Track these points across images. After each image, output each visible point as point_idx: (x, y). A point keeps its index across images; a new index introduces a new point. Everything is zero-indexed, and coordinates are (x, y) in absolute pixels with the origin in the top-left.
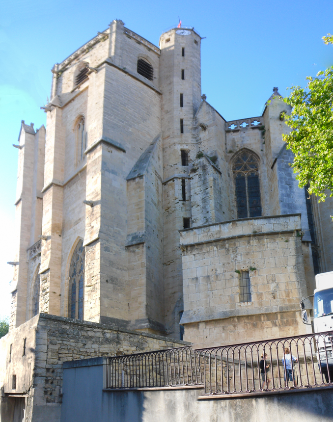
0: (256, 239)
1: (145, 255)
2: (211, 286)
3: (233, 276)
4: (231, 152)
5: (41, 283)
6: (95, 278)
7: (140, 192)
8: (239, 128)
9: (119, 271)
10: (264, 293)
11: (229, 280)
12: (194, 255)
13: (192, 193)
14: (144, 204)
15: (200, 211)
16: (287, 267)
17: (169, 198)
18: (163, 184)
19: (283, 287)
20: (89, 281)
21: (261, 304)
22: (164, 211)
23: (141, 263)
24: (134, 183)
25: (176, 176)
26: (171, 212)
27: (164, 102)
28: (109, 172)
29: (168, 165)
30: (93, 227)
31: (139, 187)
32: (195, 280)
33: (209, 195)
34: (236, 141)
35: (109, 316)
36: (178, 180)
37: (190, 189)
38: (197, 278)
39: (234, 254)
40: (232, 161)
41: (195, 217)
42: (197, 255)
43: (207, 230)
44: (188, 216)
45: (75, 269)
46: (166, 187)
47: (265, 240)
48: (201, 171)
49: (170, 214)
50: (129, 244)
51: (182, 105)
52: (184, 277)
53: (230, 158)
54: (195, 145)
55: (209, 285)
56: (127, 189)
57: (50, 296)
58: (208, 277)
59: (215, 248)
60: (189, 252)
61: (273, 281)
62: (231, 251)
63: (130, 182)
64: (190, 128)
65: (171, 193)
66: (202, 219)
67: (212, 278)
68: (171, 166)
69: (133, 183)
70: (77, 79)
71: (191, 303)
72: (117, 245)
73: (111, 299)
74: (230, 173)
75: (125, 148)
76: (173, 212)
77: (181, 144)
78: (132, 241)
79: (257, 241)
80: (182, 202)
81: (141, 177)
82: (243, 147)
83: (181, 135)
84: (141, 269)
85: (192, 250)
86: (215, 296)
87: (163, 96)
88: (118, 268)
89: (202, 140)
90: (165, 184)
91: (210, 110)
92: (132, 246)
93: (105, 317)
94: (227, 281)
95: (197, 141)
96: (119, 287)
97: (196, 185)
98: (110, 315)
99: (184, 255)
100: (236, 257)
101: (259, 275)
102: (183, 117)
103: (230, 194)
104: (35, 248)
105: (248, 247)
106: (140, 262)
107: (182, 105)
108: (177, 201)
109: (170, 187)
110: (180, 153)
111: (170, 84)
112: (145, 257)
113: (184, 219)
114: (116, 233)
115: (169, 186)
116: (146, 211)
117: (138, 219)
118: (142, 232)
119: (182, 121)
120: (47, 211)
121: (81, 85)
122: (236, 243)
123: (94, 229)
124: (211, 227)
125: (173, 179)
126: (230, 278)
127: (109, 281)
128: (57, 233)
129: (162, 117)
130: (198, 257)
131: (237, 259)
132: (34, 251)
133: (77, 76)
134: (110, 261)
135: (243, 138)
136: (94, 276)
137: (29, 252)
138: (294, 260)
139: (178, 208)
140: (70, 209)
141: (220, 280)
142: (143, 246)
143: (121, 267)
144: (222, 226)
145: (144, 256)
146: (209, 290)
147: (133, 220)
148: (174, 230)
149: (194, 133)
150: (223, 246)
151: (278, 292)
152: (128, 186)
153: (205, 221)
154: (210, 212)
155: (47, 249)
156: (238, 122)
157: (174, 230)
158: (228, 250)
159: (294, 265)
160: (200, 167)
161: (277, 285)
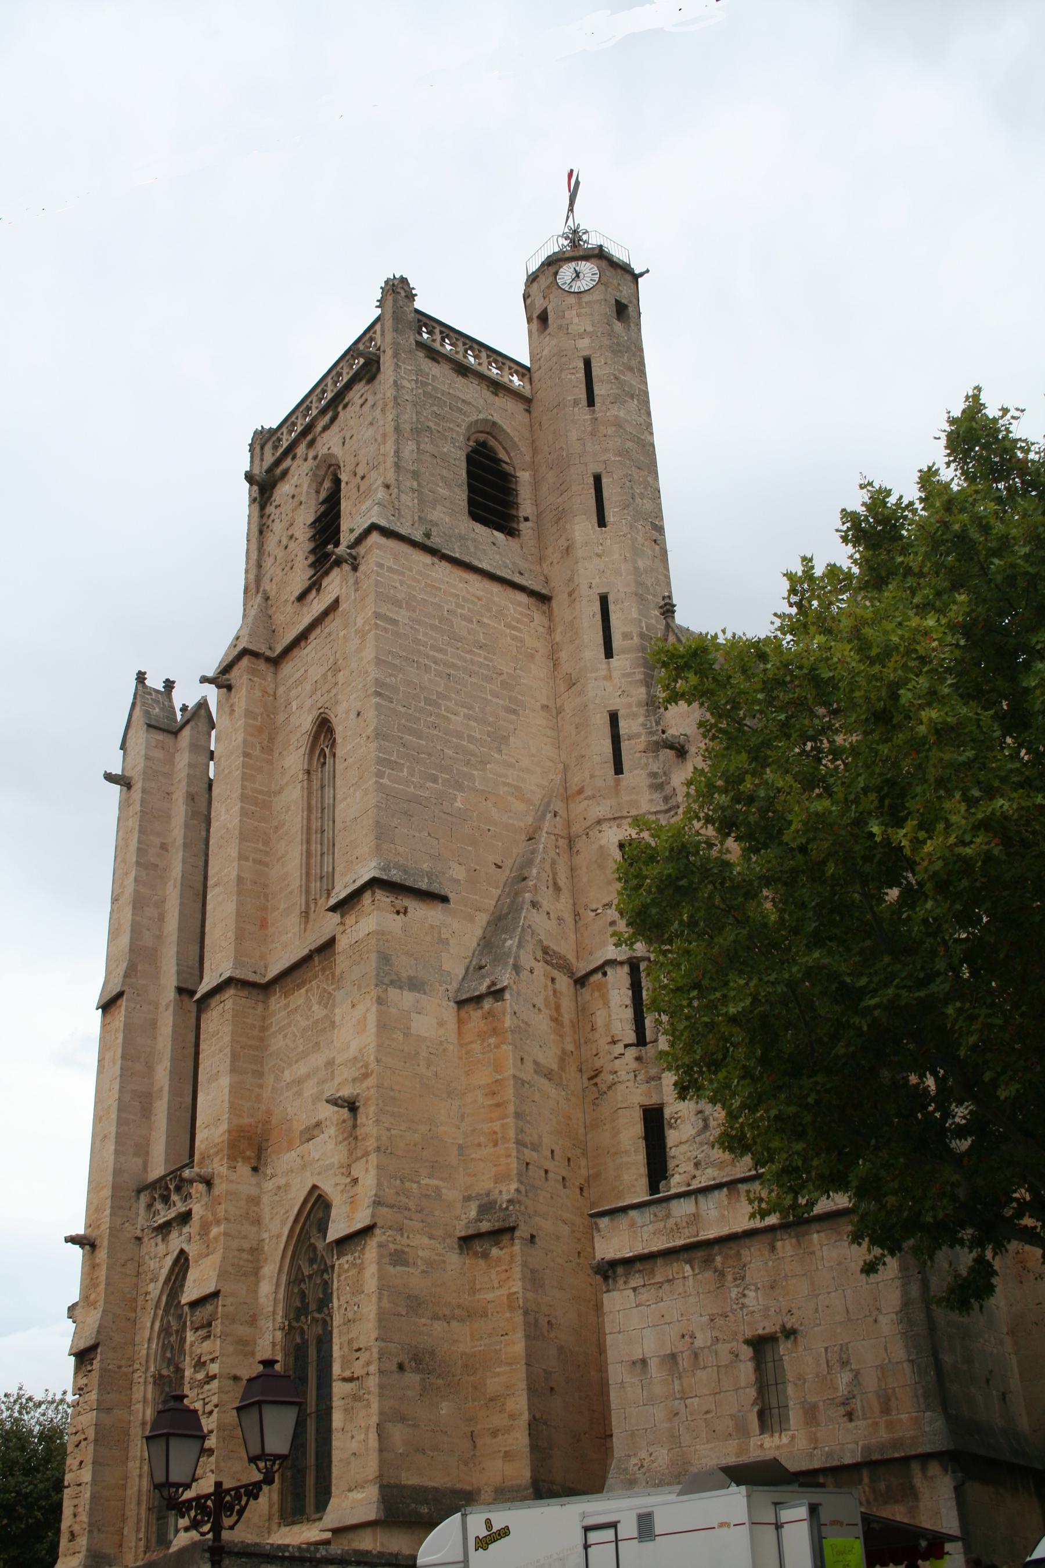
0: (790, 1237)
1: (519, 1269)
2: (682, 1385)
3: (737, 1356)
5: (190, 1337)
6: (364, 1356)
7: (497, 1047)
9: (438, 1326)
10: (821, 1404)
11: (726, 1366)
12: (634, 1289)
14: (509, 1092)
16: (880, 1318)
17: (597, 1035)
18: (576, 982)
19: (870, 1381)
20: (346, 1363)
21: (814, 1440)
22: (586, 1083)
23: (510, 1295)
24: (479, 1013)
28: (401, 988)
30: (355, 1181)
31: (495, 1031)
32: (639, 1365)
35: (410, 1482)
36: (619, 969)
38: (644, 1362)
39: (737, 1286)
42: (642, 1290)
43: (663, 1213)
44: (654, 1100)
45: (303, 1294)
46: (586, 993)
47: (815, 1236)
50: (471, 1232)
52: (611, 1355)
55: (677, 1382)
56: (460, 1033)
57: (221, 1390)
58: (673, 1356)
59: (687, 1267)
60: (621, 1281)
61: (844, 1363)
62: (730, 1277)
64: (642, 747)
66: (693, 1119)
67: (684, 1362)
69: (475, 1016)
71: (633, 1434)
72: (431, 1237)
73: (414, 1426)
79: (794, 1241)
80: (632, 1052)
81: (497, 994)
84: (508, 1315)
85: (627, 1275)
86: (691, 1414)
88: (435, 1317)
92: (479, 1236)
93: (396, 1486)
94: (723, 1370)
95: (666, 799)
96: (440, 1381)
98: (411, 1480)
99: (608, 1291)
100: (744, 1296)
101: (805, 1349)
104: (167, 1188)
105: (770, 1263)
106: (504, 1291)
108: (619, 1048)
112: (519, 1276)
114: (427, 1196)
116: (518, 1115)
117: (496, 1145)
118: (508, 1191)
119: (614, 718)
120: (214, 1078)
122: (742, 1252)
123: (359, 1189)
124: (674, 1204)
126: (731, 1362)
127: (406, 1364)
128: (246, 1159)
130: (645, 1295)
131: (746, 1301)
132: (166, 1199)
133: (314, 522)
134: (409, 1296)
136: (359, 1349)
137: (144, 1199)
138: (898, 1293)
139: (623, 1075)
140: (287, 1076)
141: (705, 1368)
142: (512, 1239)
143: (447, 1312)
144: (701, 1198)
145: (517, 1270)
146: (678, 1396)
147: (479, 1145)
148: (616, 1153)
150: (708, 1261)
151: (858, 1397)
152: (460, 1022)
153: (701, 1124)
155: (211, 1217)
157: (616, 1153)
158: (722, 1274)
159: (898, 1309)
161: (856, 1376)
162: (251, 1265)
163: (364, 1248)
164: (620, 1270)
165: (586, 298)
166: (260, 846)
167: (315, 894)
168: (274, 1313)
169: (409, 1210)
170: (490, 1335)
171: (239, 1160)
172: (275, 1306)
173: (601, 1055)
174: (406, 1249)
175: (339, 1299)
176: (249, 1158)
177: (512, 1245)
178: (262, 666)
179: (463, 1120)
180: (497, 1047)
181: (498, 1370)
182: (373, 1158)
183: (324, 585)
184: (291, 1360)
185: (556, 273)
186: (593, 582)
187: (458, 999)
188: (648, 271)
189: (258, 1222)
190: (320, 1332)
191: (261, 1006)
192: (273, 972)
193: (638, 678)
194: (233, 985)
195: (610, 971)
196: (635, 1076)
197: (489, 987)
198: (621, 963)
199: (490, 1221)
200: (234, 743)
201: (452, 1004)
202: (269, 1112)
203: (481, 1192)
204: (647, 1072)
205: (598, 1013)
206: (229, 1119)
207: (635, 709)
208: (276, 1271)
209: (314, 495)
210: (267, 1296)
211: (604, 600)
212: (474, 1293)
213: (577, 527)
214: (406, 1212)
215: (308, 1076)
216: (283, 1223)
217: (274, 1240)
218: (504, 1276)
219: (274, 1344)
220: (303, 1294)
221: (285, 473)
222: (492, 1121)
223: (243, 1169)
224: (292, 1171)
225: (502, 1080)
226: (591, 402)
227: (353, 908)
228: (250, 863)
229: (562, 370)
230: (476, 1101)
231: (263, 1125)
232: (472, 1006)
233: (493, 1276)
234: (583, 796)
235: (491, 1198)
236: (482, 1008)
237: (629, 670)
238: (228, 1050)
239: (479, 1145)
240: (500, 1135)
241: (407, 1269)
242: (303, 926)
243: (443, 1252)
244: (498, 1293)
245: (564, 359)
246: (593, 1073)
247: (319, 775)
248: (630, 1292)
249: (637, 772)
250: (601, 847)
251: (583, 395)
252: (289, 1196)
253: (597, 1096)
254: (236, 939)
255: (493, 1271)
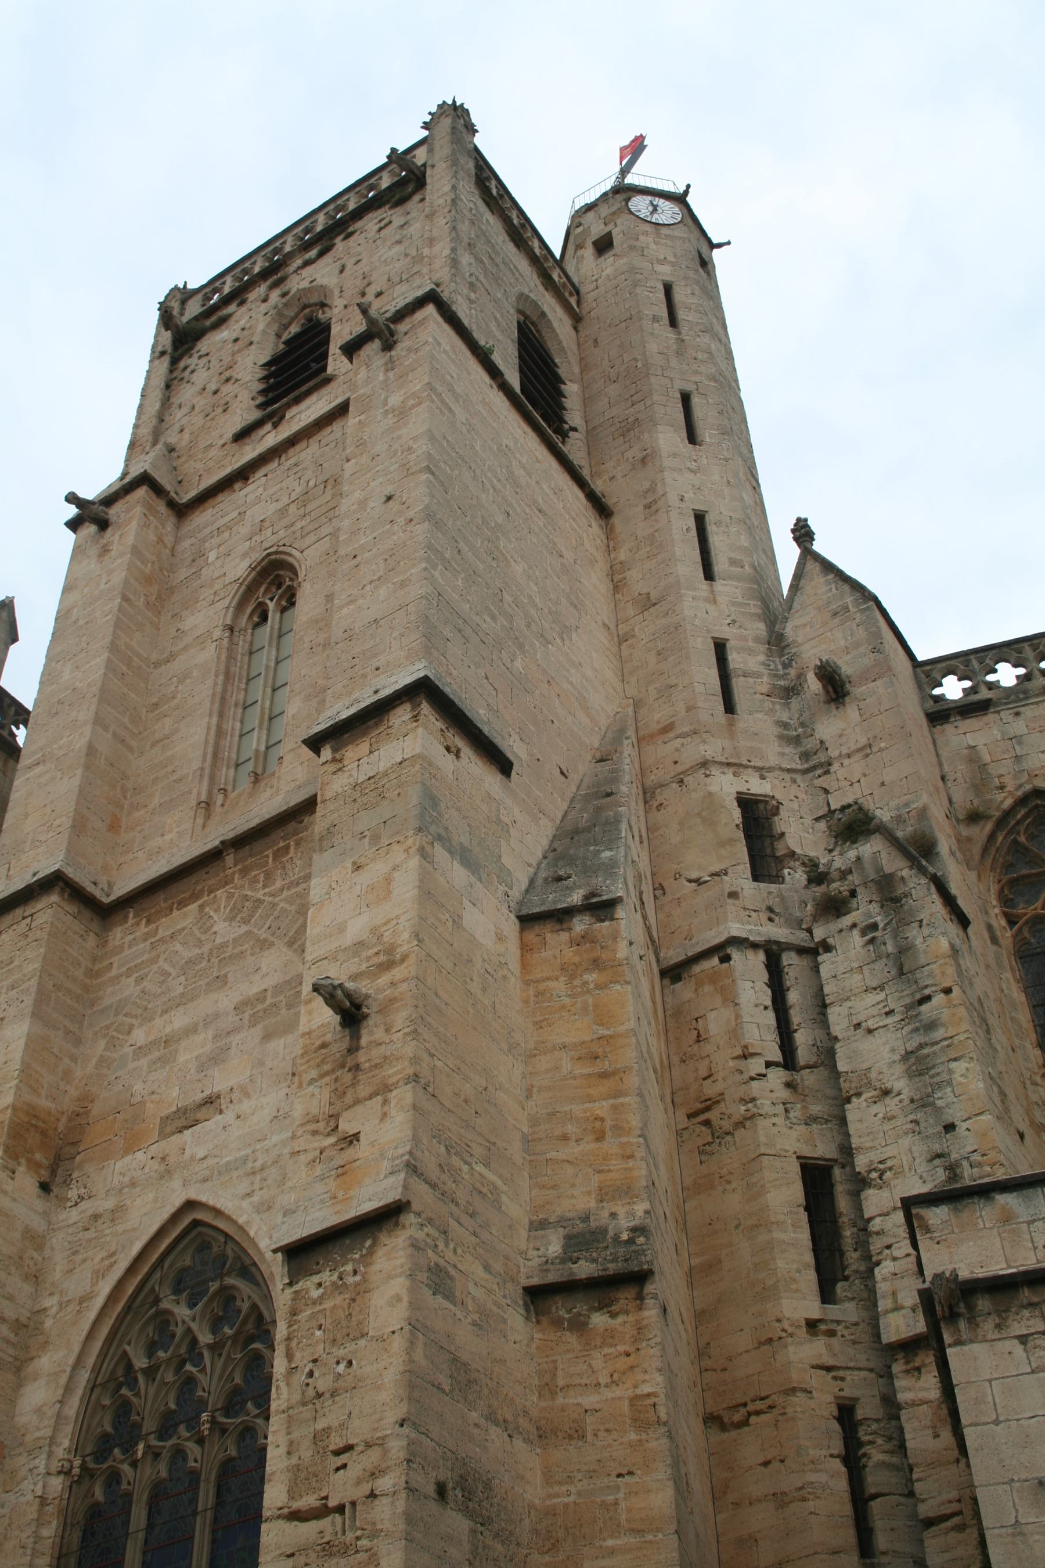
4: (974, 817)
8: (984, 694)
12: (1023, 1339)
13: (838, 1019)
15: (902, 1122)
17: (707, 1048)
18: (664, 973)
23: (634, 1400)
24: (564, 936)
25: (735, 933)
26: (727, 1125)
27: (623, 555)
29: (677, 876)
31: (596, 964)
33: (939, 1034)
34: (987, 758)
36: (750, 954)
37: (825, 1006)
40: (988, 861)
41: (874, 1156)
44: (824, 1149)
45: (123, 1408)
46: (684, 990)
48: (875, 908)
49: (719, 1136)
50: (552, 1278)
51: (709, 574)
53: (977, 849)
54: (799, 778)
56: (524, 965)
60: (988, 1326)
63: (537, 929)
64: (765, 689)
65: (716, 1023)
66: (923, 1168)
68: (698, 881)
70: (262, 392)
72: (487, 1268)
74: (995, 924)
75: (513, 747)
76: (740, 1124)
77: (735, 767)
78: (568, 1257)
82: (1028, 787)
83: (731, 724)
84: (633, 1436)
87: (616, 520)
88: (491, 1417)
89: (833, 753)
90: (673, 973)
91: (849, 600)
92: (568, 1288)
95: (805, 756)
97: (855, 981)
102: (724, 632)
103: (1017, 1041)
107: (709, 574)
108: (756, 1066)
109: (707, 988)
110: (737, 814)
111: (643, 461)
113: (804, 1168)
115: (700, 984)
117: (600, 1137)
119: (720, 648)
121: (288, 406)
125: (721, 951)
128: (34, 1166)
129: (623, 628)
133: (268, 364)
135: (1017, 739)
139: (765, 1105)
142: (640, 1297)
147: (565, 1138)
149: (785, 717)
152: (525, 948)
154: (962, 1127)
156: (975, 664)
160: (865, 884)
162: (11, 1351)
163: (371, 1252)
164: (983, 1303)
165: (665, 231)
166: (126, 720)
167: (226, 783)
168: (52, 1441)
169: (457, 1205)
170: (591, 1474)
171: (23, 1161)
172: (56, 1428)
173: (719, 1076)
174: (453, 1272)
175: (289, 1356)
176: (38, 1165)
177: (640, 1308)
178: (162, 507)
179: (529, 1097)
180: (599, 987)
181: (610, 1543)
182: (404, 1095)
183: (288, 415)
184: (76, 1536)
185: (629, 199)
186: (686, 495)
187: (524, 912)
188: (729, 243)
189: (35, 1278)
190: (164, 1474)
191: (92, 941)
192: (126, 884)
193: (753, 610)
194: (57, 889)
195: (735, 954)
196: (786, 1111)
197: (586, 897)
198: (755, 946)
199: (594, 1261)
200: (102, 586)
201: (513, 917)
202: (86, 1099)
203: (569, 1215)
204: (804, 1107)
205: (712, 1016)
206: (17, 1087)
207: (750, 644)
208: (71, 1361)
209: (273, 338)
210: (39, 1411)
211: (700, 519)
212: (553, 1394)
213: (660, 436)
214: (453, 1206)
215: (192, 1030)
216: (99, 1275)
217: (73, 1308)
218: (622, 1363)
219: (43, 1500)
220: (123, 1408)
221: (223, 321)
222: (591, 1099)
223: (27, 1182)
224: (133, 1184)
225: (611, 1037)
226: (673, 322)
227: (364, 734)
228: (109, 736)
229: (635, 285)
230: (557, 1068)
231: (70, 1120)
232: (550, 925)
233: (598, 1362)
234: (671, 735)
235: (593, 1224)
236: (570, 929)
237: (740, 599)
238: (34, 982)
239: (565, 1138)
240: (609, 1123)
241: (452, 1307)
242: (200, 821)
243: (503, 1302)
244: (608, 1393)
245: (638, 276)
246: (699, 1106)
247: (249, 638)
248: (1018, 1350)
249: (760, 716)
250: (710, 794)
251: (664, 313)
252: (120, 1228)
253: (710, 1139)
254: (73, 827)
255: (596, 1354)
